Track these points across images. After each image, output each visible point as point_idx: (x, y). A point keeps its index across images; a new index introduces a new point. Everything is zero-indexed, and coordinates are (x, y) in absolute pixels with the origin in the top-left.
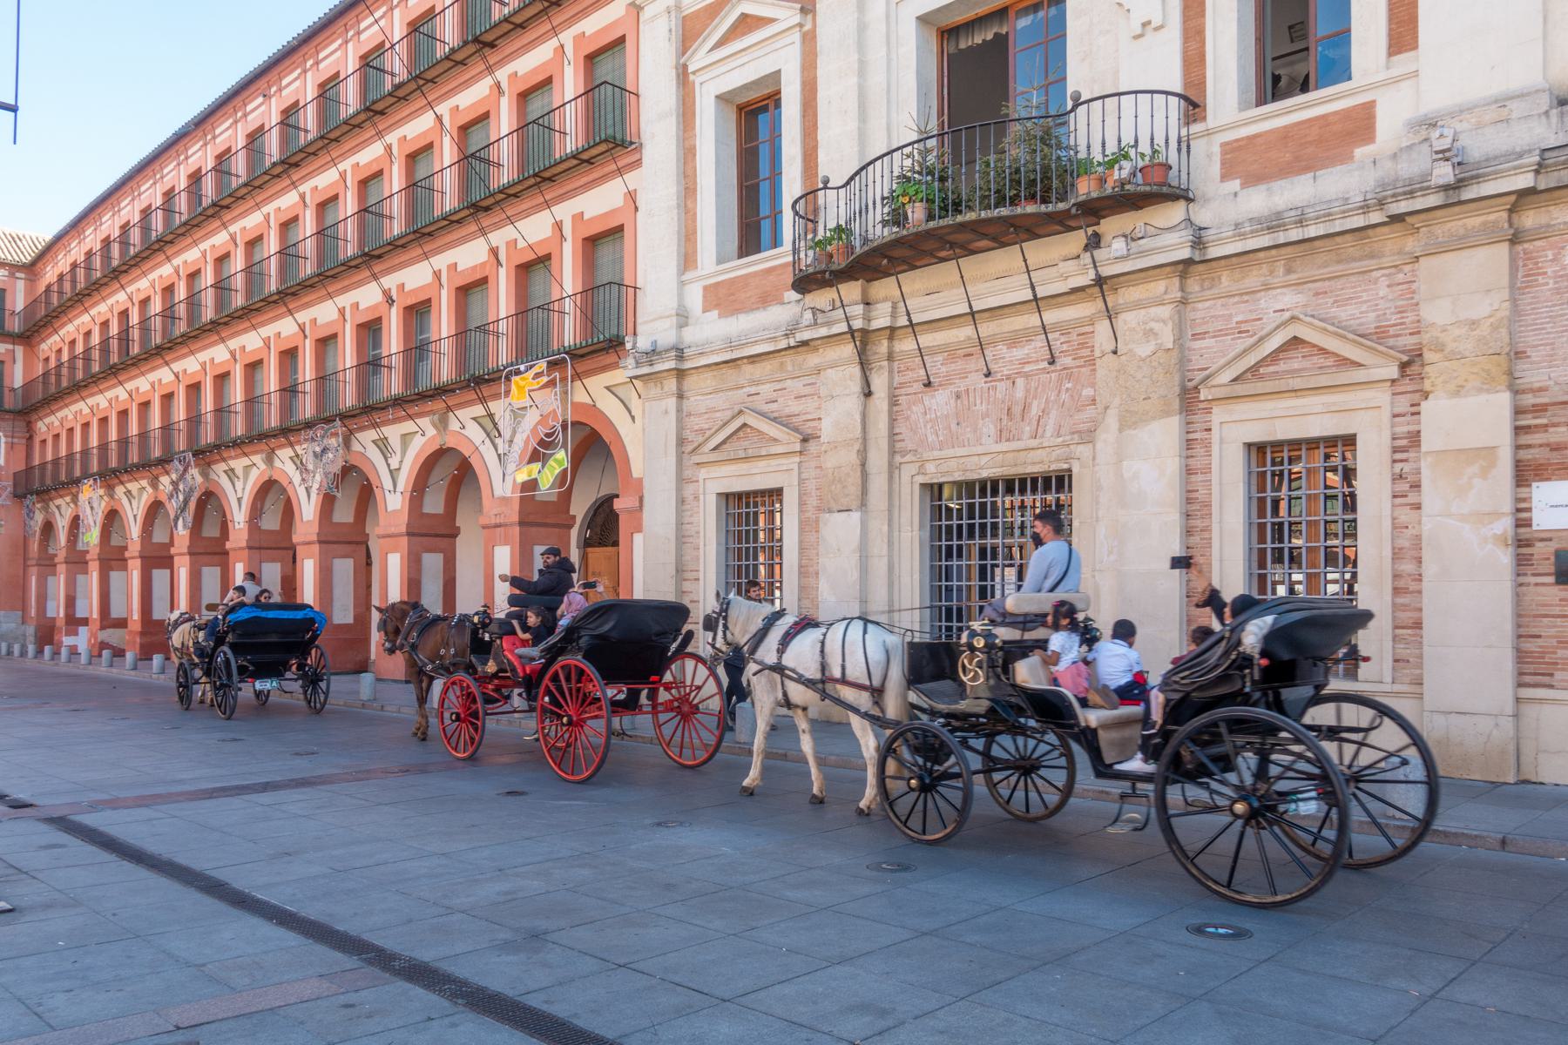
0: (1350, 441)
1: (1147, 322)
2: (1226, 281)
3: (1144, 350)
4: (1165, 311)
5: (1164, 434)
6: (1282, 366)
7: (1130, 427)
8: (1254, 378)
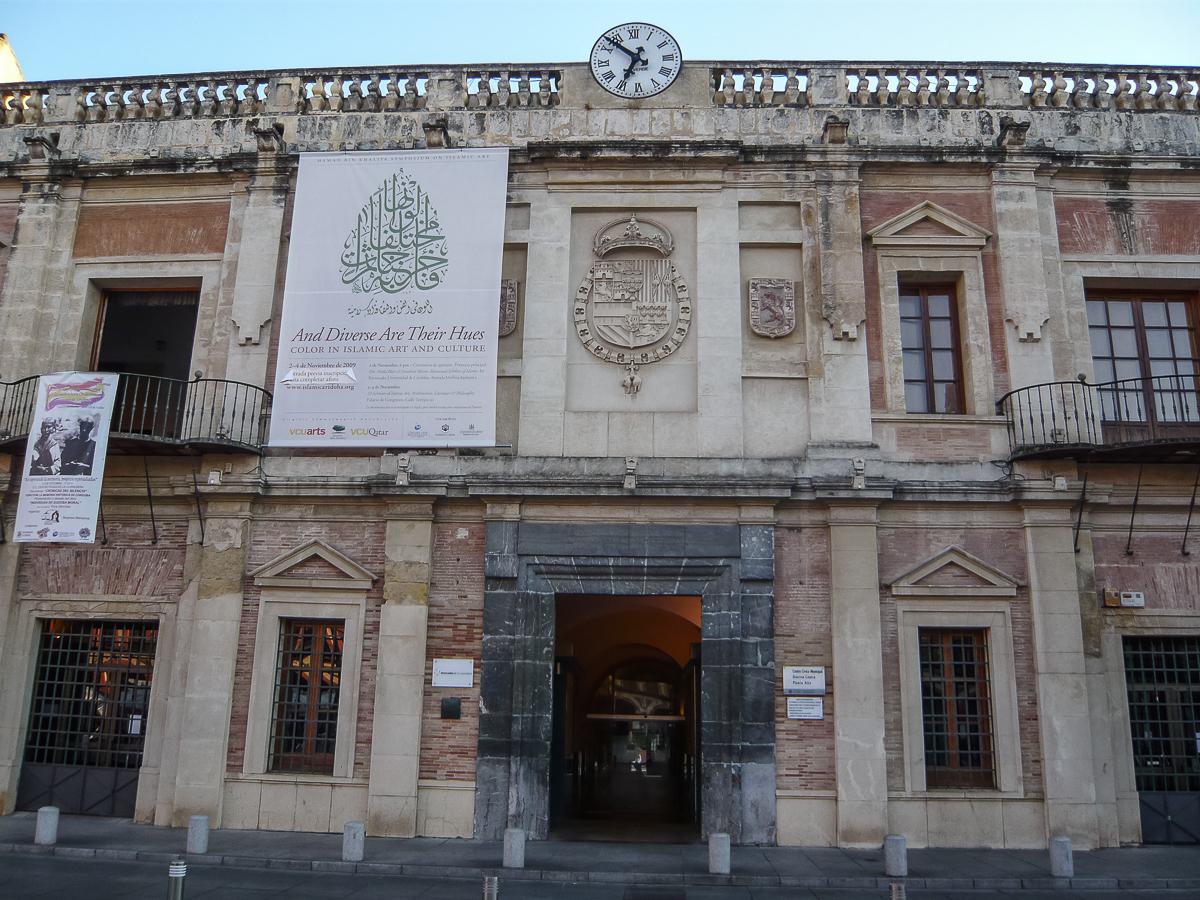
0: (981, 633)
1: (224, 532)
2: (279, 512)
3: (221, 546)
4: (236, 523)
5: (230, 604)
6: (308, 570)
7: (208, 596)
8: (288, 577)
